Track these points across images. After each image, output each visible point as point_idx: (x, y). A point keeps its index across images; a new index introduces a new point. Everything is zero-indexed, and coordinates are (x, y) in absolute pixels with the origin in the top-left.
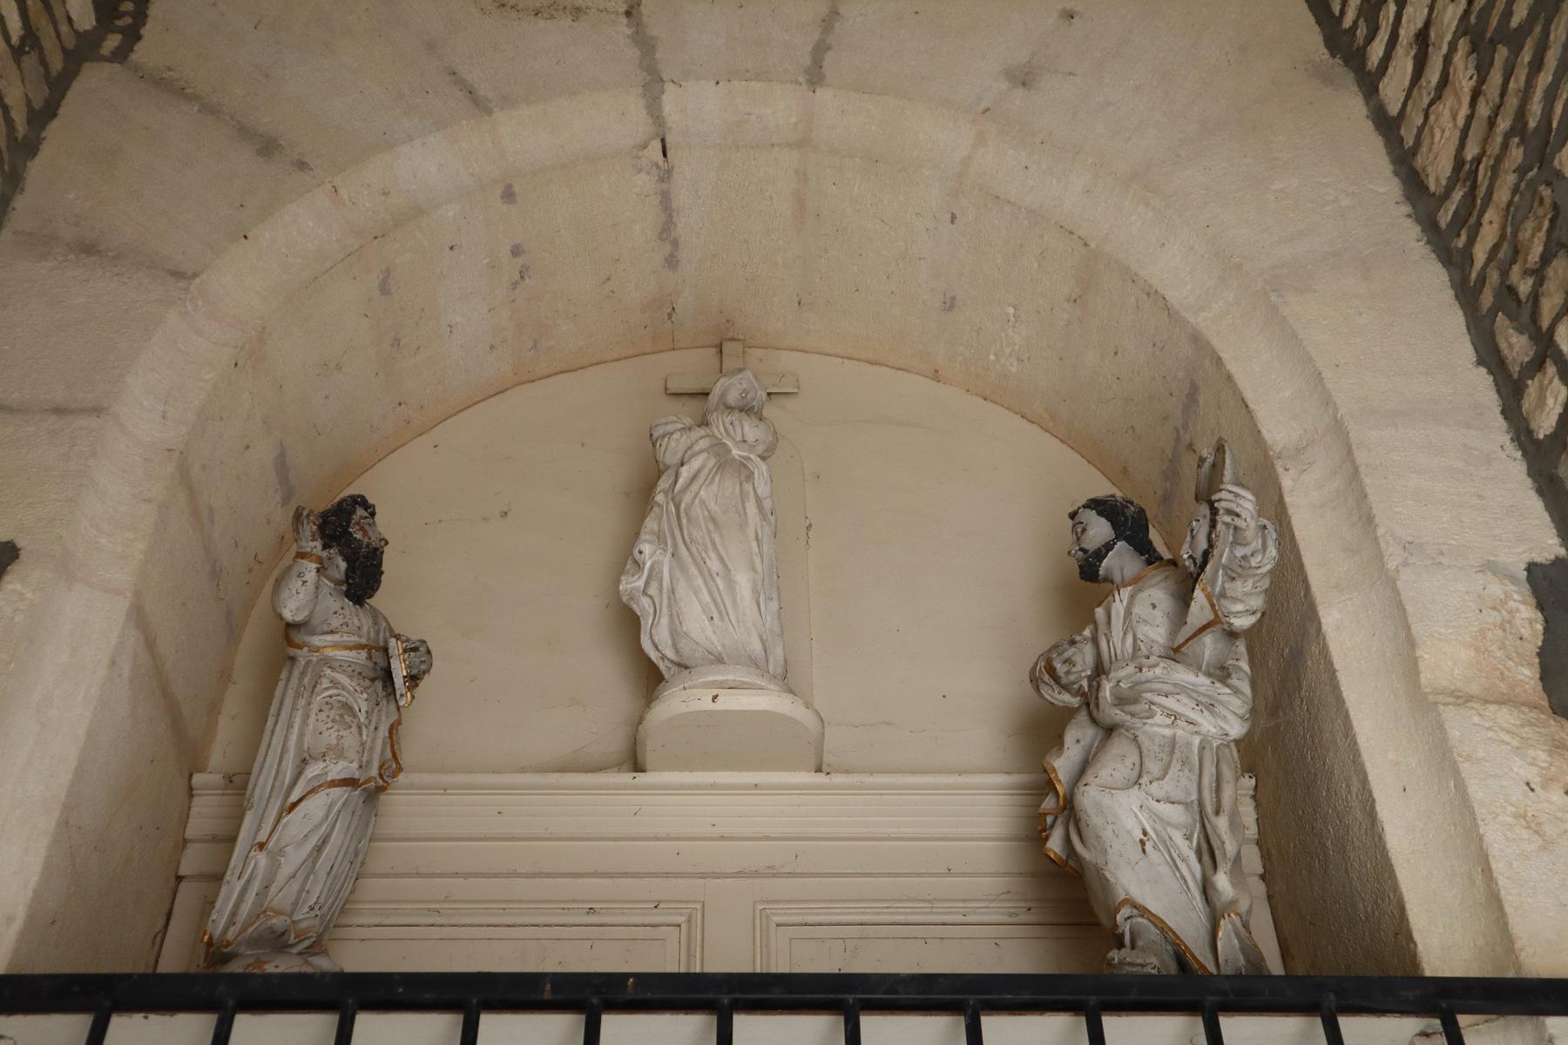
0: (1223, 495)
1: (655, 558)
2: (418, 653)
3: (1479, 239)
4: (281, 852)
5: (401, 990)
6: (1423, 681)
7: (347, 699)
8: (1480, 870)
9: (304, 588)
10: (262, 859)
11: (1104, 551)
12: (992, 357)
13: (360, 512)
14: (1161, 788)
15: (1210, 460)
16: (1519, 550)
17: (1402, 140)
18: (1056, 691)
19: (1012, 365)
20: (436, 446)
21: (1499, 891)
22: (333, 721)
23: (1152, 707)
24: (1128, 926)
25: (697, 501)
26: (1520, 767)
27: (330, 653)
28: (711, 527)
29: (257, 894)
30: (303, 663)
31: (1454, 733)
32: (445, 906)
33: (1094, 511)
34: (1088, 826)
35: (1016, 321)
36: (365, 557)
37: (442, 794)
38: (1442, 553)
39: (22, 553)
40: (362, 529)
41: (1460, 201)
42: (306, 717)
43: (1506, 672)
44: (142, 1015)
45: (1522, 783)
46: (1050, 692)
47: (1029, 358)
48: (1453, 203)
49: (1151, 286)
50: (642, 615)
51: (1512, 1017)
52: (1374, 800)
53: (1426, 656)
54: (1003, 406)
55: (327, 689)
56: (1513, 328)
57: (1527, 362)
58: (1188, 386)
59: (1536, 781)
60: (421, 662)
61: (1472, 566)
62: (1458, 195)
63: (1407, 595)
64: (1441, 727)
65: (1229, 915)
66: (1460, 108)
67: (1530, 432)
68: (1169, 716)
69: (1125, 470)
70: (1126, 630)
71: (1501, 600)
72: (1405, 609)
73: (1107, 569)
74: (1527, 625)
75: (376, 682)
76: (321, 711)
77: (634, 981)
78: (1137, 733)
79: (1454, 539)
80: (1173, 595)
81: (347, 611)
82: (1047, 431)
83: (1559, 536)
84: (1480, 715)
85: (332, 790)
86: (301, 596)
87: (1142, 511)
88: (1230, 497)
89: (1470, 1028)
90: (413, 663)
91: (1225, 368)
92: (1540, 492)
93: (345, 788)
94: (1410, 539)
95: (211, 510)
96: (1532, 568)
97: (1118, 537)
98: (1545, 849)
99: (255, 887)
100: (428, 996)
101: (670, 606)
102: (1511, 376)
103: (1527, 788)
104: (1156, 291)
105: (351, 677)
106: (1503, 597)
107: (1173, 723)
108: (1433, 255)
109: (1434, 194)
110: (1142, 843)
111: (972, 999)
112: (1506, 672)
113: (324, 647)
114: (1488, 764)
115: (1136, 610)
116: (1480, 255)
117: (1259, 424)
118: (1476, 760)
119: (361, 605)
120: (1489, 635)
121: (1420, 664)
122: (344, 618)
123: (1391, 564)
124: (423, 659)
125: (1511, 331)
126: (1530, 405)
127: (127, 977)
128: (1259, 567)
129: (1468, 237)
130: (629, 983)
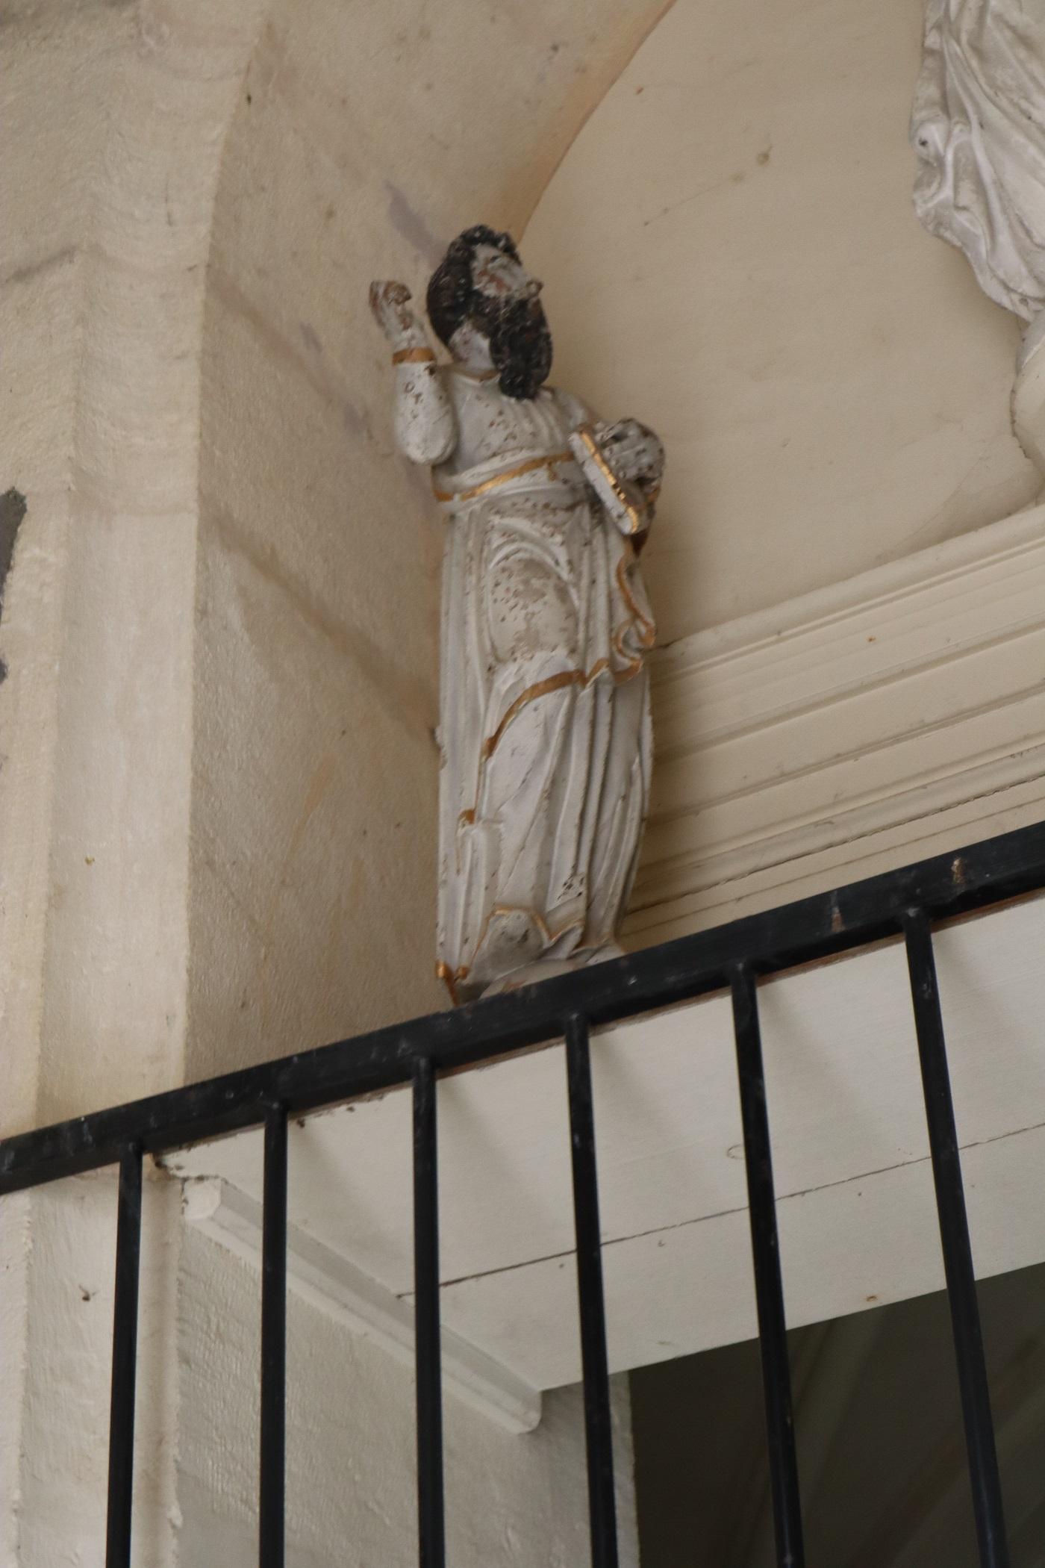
1: (954, 143)
2: (625, 443)
4: (496, 819)
5: (633, 981)
7: (532, 552)
9: (420, 406)
10: (478, 834)
13: (483, 252)
20: (640, 91)
22: (516, 594)
25: (989, 20)
27: (492, 489)
28: (1023, 53)
29: (486, 888)
30: (466, 519)
32: (839, 810)
36: (509, 320)
37: (778, 641)
39: (29, 503)
40: (493, 278)
42: (480, 601)
44: (343, 1108)
50: (964, 244)
55: (499, 547)
60: (638, 453)
75: (578, 510)
76: (497, 585)
77: (961, 862)
81: (509, 415)
85: (540, 699)
86: (421, 418)
90: (622, 461)
93: (559, 691)
95: (310, 336)
99: (482, 877)
100: (671, 979)
101: (1004, 211)
105: (531, 517)
113: (481, 485)
119: (533, 397)
122: (507, 427)
124: (640, 447)
127: (284, 1063)
130: (954, 868)
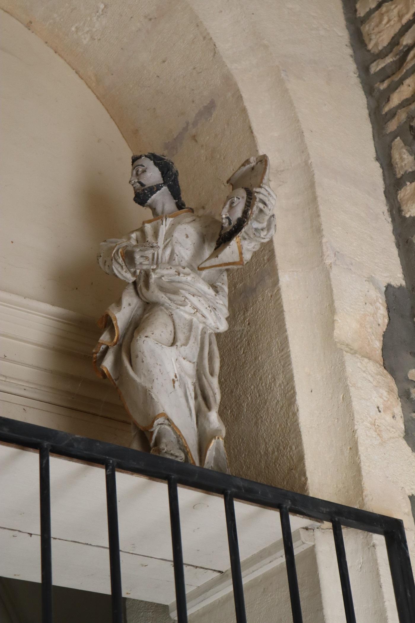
0: (262, 190)
3: (397, 91)
6: (335, 334)
8: (349, 448)
11: (155, 189)
12: (73, 29)
14: (185, 351)
15: (253, 164)
16: (385, 275)
17: (356, 11)
18: (124, 270)
19: (85, 39)
21: (360, 462)
23: (186, 300)
24: (158, 429)
26: (376, 397)
31: (349, 369)
33: (152, 161)
34: (143, 362)
35: (102, 14)
38: (352, 264)
41: (389, 63)
43: (371, 341)
45: (376, 407)
46: (120, 269)
47: (100, 39)
48: (384, 63)
49: (208, 34)
51: (352, 529)
52: (295, 393)
53: (339, 321)
54: (65, 60)
56: (407, 150)
57: (410, 172)
58: (208, 102)
59: (381, 407)
61: (364, 277)
62: (389, 60)
63: (334, 283)
64: (343, 364)
65: (218, 438)
66: (407, 13)
67: (400, 211)
68: (194, 308)
69: (136, 132)
70: (167, 244)
71: (374, 300)
72: (332, 290)
73: (153, 201)
74: (382, 318)
78: (173, 313)
79: (358, 258)
80: (198, 233)
82: (89, 87)
83: (403, 274)
84: (361, 363)
87: (177, 171)
88: (266, 193)
89: (328, 530)
91: (243, 104)
92: (398, 246)
94: (338, 250)
96: (389, 287)
97: (165, 183)
98: (382, 445)
102: (395, 175)
103: (377, 409)
104: (211, 39)
106: (375, 299)
107: (195, 313)
108: (360, 85)
109: (369, 51)
110: (174, 381)
111: (46, 444)
112: (371, 341)
114: (362, 391)
115: (176, 235)
116: (396, 99)
117: (258, 146)
118: (358, 388)
120: (368, 318)
121: (336, 324)
123: (328, 261)
125: (404, 151)
126: (404, 196)
128: (264, 238)
129: (389, 86)
